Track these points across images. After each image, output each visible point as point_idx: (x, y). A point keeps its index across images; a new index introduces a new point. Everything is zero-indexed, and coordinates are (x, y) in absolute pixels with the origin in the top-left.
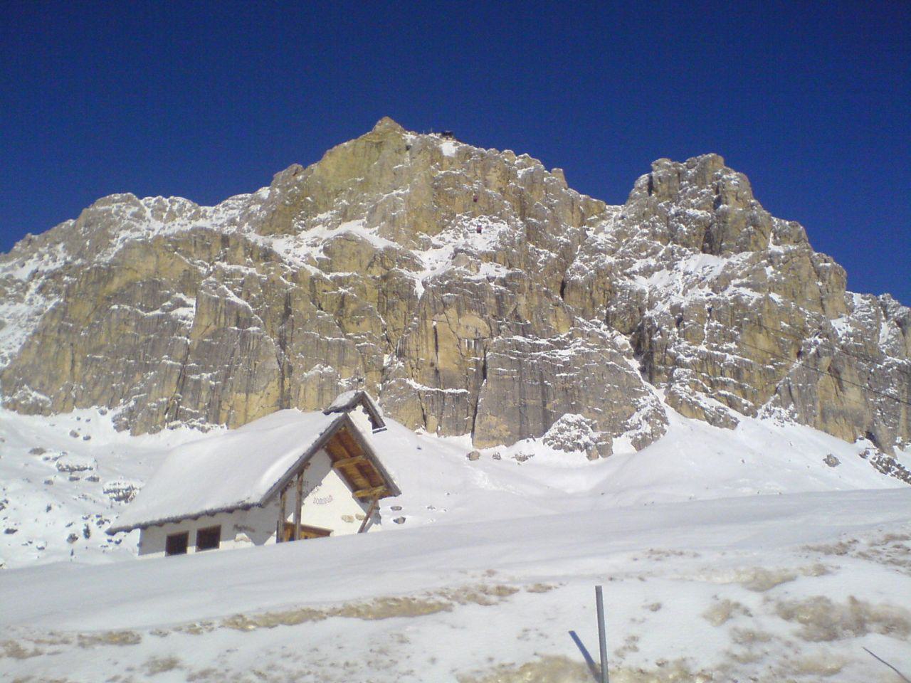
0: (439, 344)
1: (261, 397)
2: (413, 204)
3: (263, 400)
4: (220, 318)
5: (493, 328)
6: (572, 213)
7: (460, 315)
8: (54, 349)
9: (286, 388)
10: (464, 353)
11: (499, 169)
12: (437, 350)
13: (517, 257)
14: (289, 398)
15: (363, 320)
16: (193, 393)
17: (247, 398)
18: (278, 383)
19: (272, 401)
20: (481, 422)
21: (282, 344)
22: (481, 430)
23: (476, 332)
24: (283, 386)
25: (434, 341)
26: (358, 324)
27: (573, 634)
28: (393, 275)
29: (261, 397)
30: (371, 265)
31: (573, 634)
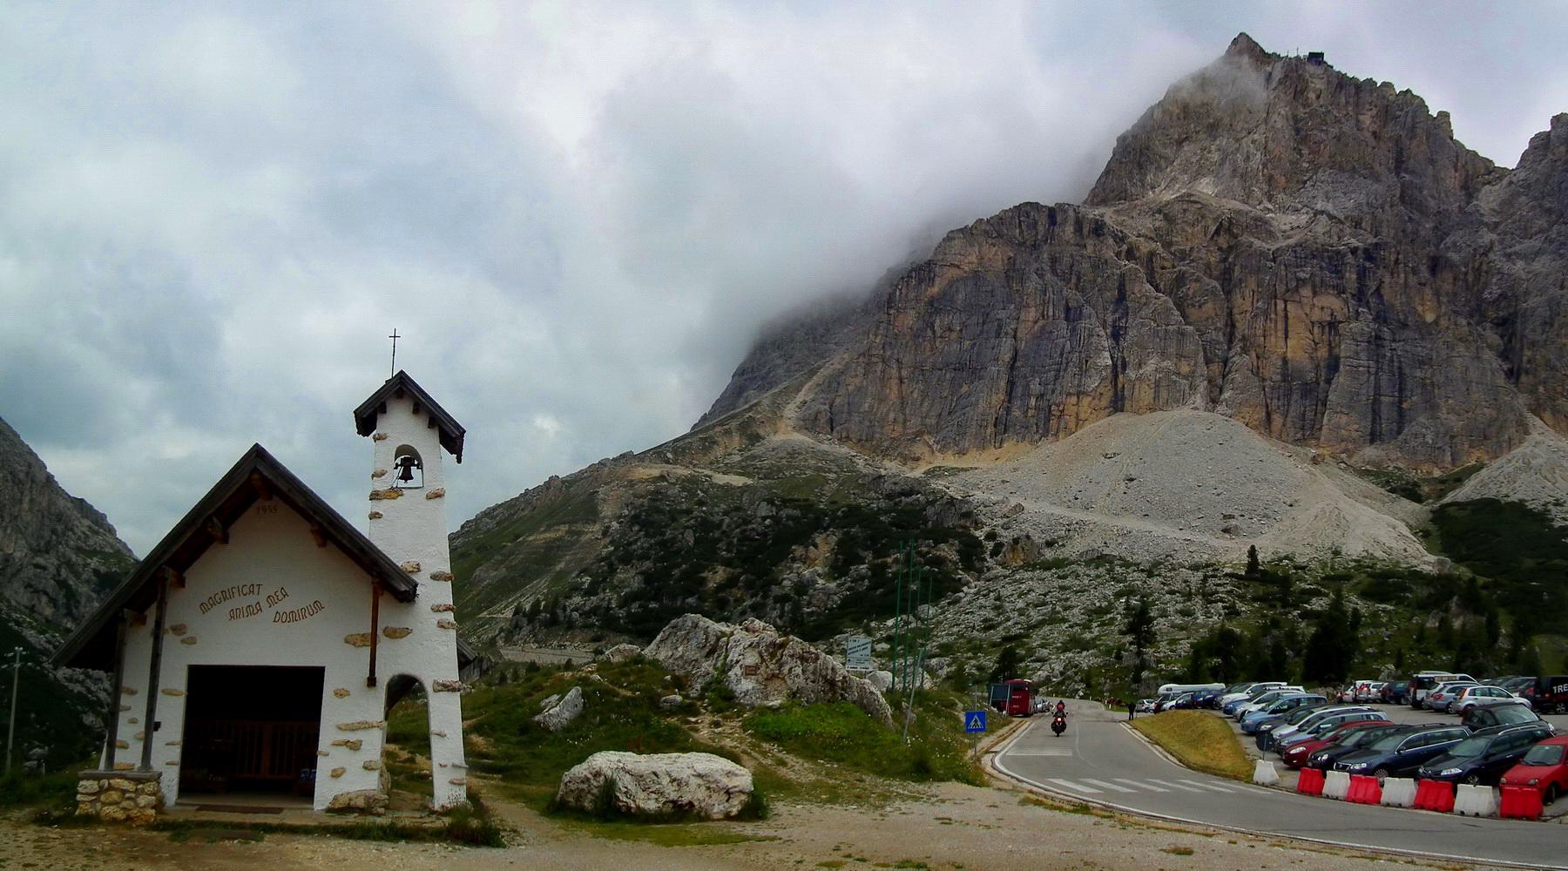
0: (1289, 329)
1: (1094, 399)
2: (1269, 151)
3: (1096, 401)
4: (1048, 311)
5: (1351, 310)
6: (1456, 171)
7: (1315, 294)
8: (880, 367)
9: (1120, 386)
10: (1317, 341)
11: (1376, 107)
12: (1286, 337)
13: (1386, 223)
14: (1123, 399)
15: (1206, 302)
16: (1021, 400)
17: (1078, 402)
18: (1111, 383)
19: (1105, 402)
20: (1329, 420)
21: (1116, 335)
22: (1330, 430)
23: (1332, 315)
24: (1116, 385)
25: (1284, 326)
26: (1200, 307)
27: (167, 764)
28: (1242, 245)
29: (1094, 399)
30: (1217, 232)
31: (168, 744)
